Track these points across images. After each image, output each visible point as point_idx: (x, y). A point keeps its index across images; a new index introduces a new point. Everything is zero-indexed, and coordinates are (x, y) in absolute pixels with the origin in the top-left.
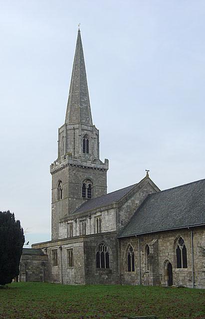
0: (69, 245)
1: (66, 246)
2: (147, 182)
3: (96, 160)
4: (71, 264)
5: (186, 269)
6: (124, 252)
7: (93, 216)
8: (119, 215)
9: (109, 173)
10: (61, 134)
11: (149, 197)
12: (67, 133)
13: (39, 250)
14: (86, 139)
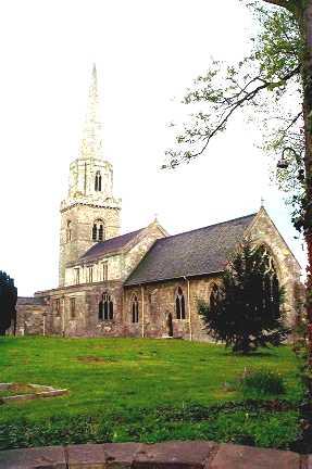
13: (42, 299)
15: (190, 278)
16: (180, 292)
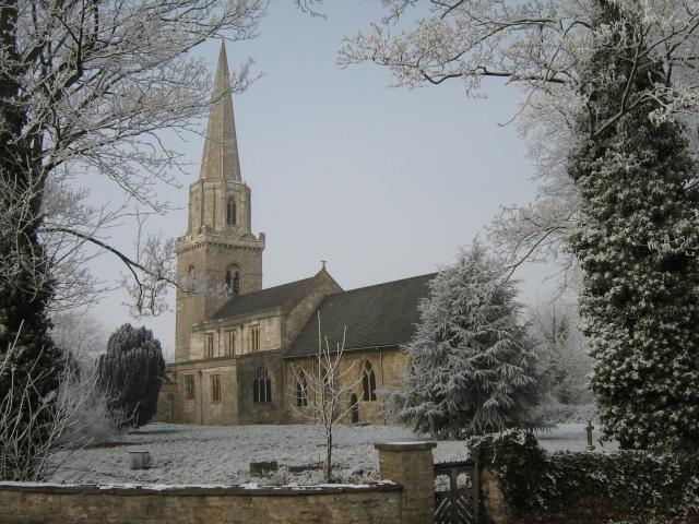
0: (214, 369)
1: (208, 371)
2: (323, 277)
3: (248, 235)
4: (216, 396)
5: (375, 402)
6: (293, 376)
7: (246, 325)
8: (285, 326)
9: (265, 254)
10: (195, 196)
11: (326, 299)
12: (203, 194)
14: (232, 204)
15: (381, 350)
16: (369, 366)
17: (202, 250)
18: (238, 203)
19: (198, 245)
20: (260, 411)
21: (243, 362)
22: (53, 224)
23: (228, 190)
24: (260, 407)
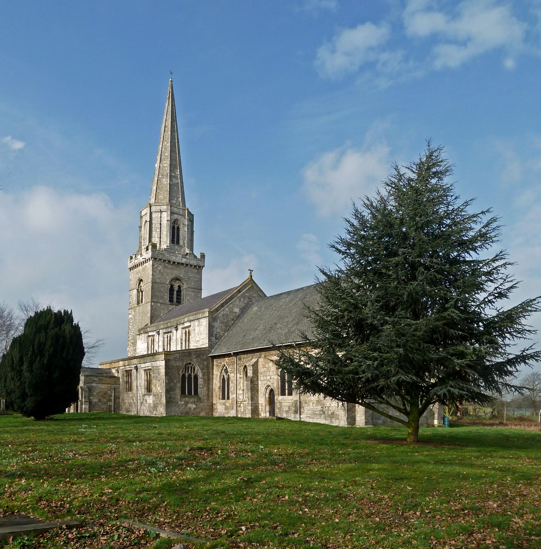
7: (180, 327)
17: (150, 264)
18: (181, 227)
19: (146, 261)
20: (186, 403)
21: (172, 357)
22: (327, 490)
23: (172, 213)
24: (187, 399)
